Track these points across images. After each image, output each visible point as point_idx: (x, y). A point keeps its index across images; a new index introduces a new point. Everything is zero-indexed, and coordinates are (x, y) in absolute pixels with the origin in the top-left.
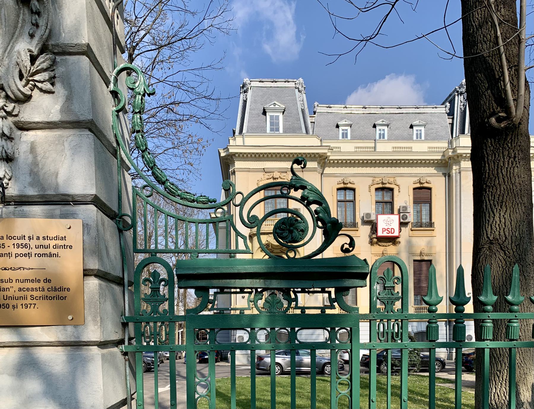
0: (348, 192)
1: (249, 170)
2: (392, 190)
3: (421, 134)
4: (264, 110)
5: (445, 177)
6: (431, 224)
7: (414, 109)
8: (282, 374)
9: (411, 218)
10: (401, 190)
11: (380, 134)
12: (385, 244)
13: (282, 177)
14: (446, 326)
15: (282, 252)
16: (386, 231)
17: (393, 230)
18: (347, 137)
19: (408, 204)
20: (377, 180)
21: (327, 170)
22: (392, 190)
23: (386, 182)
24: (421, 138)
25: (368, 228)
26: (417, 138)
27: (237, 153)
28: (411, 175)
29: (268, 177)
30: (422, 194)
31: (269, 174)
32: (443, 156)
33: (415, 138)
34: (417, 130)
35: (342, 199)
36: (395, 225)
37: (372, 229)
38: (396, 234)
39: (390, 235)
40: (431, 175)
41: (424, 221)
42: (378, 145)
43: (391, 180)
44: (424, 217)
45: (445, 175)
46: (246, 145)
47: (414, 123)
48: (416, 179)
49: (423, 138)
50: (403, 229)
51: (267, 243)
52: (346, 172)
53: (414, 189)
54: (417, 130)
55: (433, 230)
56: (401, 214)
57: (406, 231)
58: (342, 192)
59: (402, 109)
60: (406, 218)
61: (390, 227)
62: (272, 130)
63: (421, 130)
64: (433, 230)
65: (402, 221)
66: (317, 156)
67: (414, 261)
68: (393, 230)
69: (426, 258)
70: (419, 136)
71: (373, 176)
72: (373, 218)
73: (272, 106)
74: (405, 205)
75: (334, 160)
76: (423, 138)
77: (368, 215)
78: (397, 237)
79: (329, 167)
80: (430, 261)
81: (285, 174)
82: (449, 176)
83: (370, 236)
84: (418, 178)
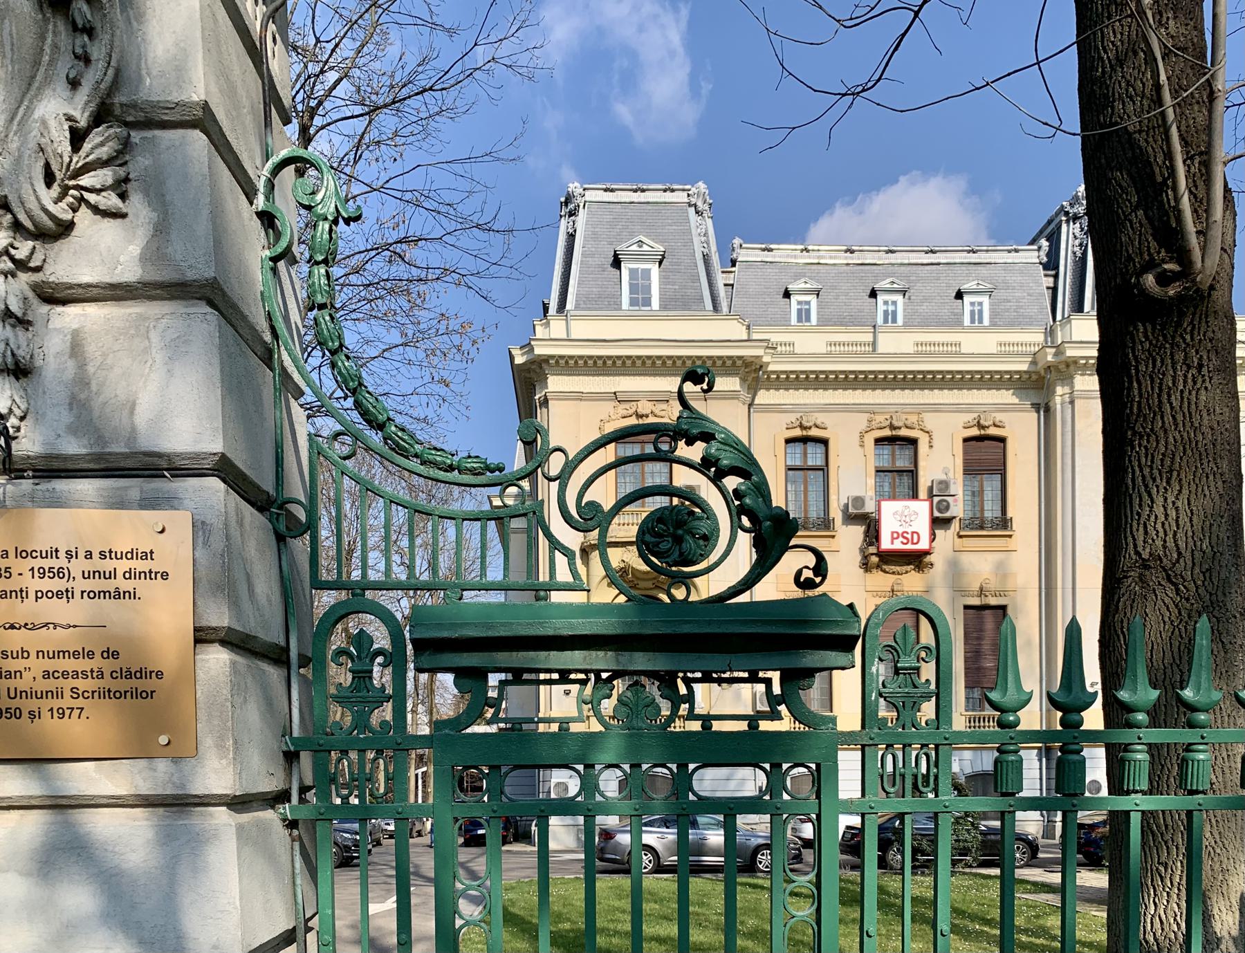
0: (811, 448)
1: (580, 397)
2: (913, 442)
3: (981, 312)
4: (616, 256)
5: (1038, 412)
6: (1004, 523)
7: (965, 254)
9: (958, 509)
10: (934, 443)
11: (886, 312)
12: (898, 568)
13: (657, 412)
14: (1040, 760)
15: (657, 587)
16: (901, 539)
17: (915, 536)
18: (808, 319)
19: (951, 475)
20: (880, 418)
21: (763, 397)
22: (913, 442)
23: (900, 424)
24: (981, 321)
25: (858, 531)
26: (973, 321)
27: (552, 357)
28: (957, 408)
29: (625, 413)
30: (985, 453)
31: (627, 406)
32: (1034, 363)
33: (967, 321)
34: (972, 304)
35: (798, 463)
36: (922, 525)
37: (867, 533)
38: (924, 545)
39: (909, 547)
40: (1005, 408)
41: (988, 514)
42: (880, 337)
43: (913, 419)
44: (988, 506)
45: (1036, 407)
46: (573, 337)
47: (966, 286)
48: (970, 417)
49: (986, 322)
50: (940, 533)
51: (622, 565)
52: (807, 402)
53: (966, 440)
54: (972, 304)
55: (1010, 536)
56: (936, 499)
57: (946, 538)
58: (799, 447)
59: (938, 255)
60: (947, 508)
61: (910, 530)
62: (633, 302)
63: (980, 304)
64: (1010, 536)
65: (936, 514)
66: (739, 363)
67: (966, 607)
68: (915, 536)
69: (993, 601)
70: (976, 316)
71: (871, 410)
72: (870, 507)
73: (635, 247)
74: (944, 477)
75: (778, 373)
76: (986, 322)
77: (859, 501)
78: (927, 553)
79: (768, 389)
80: (1003, 608)
81: (664, 406)
82: (1048, 410)
83: (862, 550)
84: (976, 415)
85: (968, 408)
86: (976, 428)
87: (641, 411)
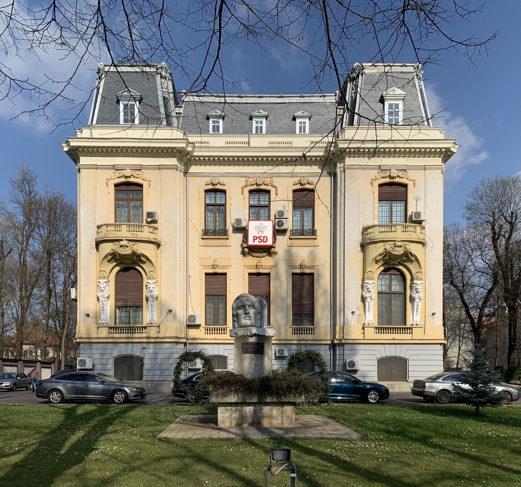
0: (219, 195)
1: (96, 167)
2: (268, 192)
3: (304, 127)
4: (208, 117)
5: (331, 177)
6: (313, 232)
7: (298, 98)
8: (61, 402)
9: (288, 225)
10: (278, 193)
11: (257, 127)
12: (259, 255)
13: (135, 175)
14: (330, 351)
15: (134, 263)
16: (258, 240)
17: (265, 238)
18: (218, 131)
19: (286, 209)
20: (251, 180)
21: (193, 169)
22: (268, 192)
23: (261, 183)
24: (304, 131)
25: (240, 236)
26: (300, 132)
27: (80, 147)
28: (292, 175)
29: (119, 175)
30: (304, 198)
31: (120, 172)
32: (326, 151)
33: (298, 131)
34: (300, 123)
35: (213, 202)
36: (269, 233)
37: (244, 236)
38: (270, 242)
39: (262, 243)
40: (313, 175)
41: (306, 228)
42: (252, 139)
43: (268, 181)
44: (306, 224)
45: (330, 174)
46: (93, 137)
47: (296, 114)
48: (296, 180)
49: (307, 132)
50: (279, 238)
51: (112, 251)
52: (216, 171)
53: (294, 191)
54: (300, 123)
55: (316, 239)
56: (277, 220)
57: (282, 241)
58: (213, 195)
59: (285, 98)
60: (283, 224)
61: (262, 235)
62: (126, 121)
63: (304, 123)
64: (316, 239)
65: (277, 227)
66: (175, 151)
67: (293, 274)
68: (265, 238)
69: (307, 271)
70: (302, 129)
71: (246, 176)
72: (244, 224)
73: (214, 114)
74: (282, 209)
75: (199, 157)
76: (307, 132)
77: (239, 221)
78: (271, 247)
79: (196, 165)
80: (312, 274)
81: (139, 172)
82: (335, 176)
83: (242, 245)
84: (299, 178)
85: (209, 175)
86: (388, 178)
87: (392, 175)
